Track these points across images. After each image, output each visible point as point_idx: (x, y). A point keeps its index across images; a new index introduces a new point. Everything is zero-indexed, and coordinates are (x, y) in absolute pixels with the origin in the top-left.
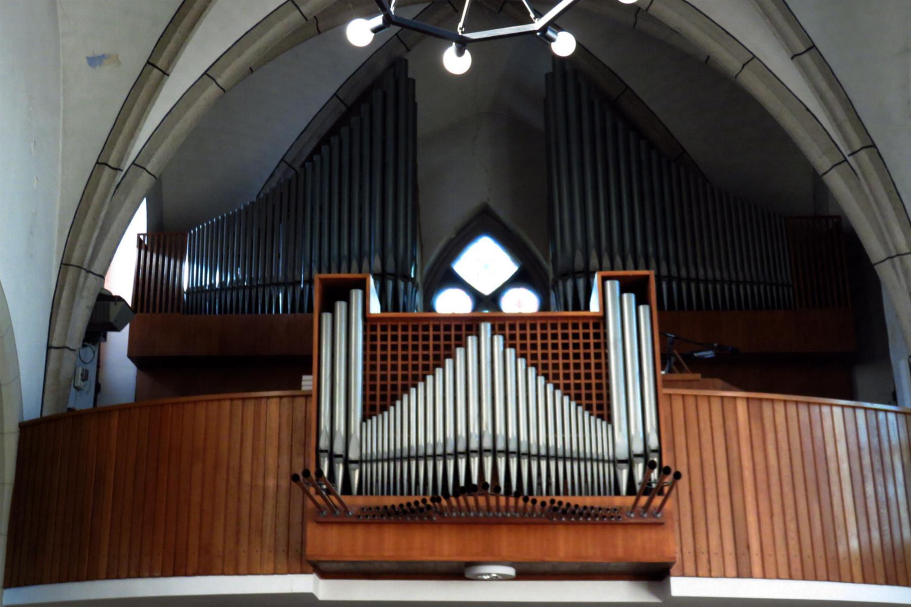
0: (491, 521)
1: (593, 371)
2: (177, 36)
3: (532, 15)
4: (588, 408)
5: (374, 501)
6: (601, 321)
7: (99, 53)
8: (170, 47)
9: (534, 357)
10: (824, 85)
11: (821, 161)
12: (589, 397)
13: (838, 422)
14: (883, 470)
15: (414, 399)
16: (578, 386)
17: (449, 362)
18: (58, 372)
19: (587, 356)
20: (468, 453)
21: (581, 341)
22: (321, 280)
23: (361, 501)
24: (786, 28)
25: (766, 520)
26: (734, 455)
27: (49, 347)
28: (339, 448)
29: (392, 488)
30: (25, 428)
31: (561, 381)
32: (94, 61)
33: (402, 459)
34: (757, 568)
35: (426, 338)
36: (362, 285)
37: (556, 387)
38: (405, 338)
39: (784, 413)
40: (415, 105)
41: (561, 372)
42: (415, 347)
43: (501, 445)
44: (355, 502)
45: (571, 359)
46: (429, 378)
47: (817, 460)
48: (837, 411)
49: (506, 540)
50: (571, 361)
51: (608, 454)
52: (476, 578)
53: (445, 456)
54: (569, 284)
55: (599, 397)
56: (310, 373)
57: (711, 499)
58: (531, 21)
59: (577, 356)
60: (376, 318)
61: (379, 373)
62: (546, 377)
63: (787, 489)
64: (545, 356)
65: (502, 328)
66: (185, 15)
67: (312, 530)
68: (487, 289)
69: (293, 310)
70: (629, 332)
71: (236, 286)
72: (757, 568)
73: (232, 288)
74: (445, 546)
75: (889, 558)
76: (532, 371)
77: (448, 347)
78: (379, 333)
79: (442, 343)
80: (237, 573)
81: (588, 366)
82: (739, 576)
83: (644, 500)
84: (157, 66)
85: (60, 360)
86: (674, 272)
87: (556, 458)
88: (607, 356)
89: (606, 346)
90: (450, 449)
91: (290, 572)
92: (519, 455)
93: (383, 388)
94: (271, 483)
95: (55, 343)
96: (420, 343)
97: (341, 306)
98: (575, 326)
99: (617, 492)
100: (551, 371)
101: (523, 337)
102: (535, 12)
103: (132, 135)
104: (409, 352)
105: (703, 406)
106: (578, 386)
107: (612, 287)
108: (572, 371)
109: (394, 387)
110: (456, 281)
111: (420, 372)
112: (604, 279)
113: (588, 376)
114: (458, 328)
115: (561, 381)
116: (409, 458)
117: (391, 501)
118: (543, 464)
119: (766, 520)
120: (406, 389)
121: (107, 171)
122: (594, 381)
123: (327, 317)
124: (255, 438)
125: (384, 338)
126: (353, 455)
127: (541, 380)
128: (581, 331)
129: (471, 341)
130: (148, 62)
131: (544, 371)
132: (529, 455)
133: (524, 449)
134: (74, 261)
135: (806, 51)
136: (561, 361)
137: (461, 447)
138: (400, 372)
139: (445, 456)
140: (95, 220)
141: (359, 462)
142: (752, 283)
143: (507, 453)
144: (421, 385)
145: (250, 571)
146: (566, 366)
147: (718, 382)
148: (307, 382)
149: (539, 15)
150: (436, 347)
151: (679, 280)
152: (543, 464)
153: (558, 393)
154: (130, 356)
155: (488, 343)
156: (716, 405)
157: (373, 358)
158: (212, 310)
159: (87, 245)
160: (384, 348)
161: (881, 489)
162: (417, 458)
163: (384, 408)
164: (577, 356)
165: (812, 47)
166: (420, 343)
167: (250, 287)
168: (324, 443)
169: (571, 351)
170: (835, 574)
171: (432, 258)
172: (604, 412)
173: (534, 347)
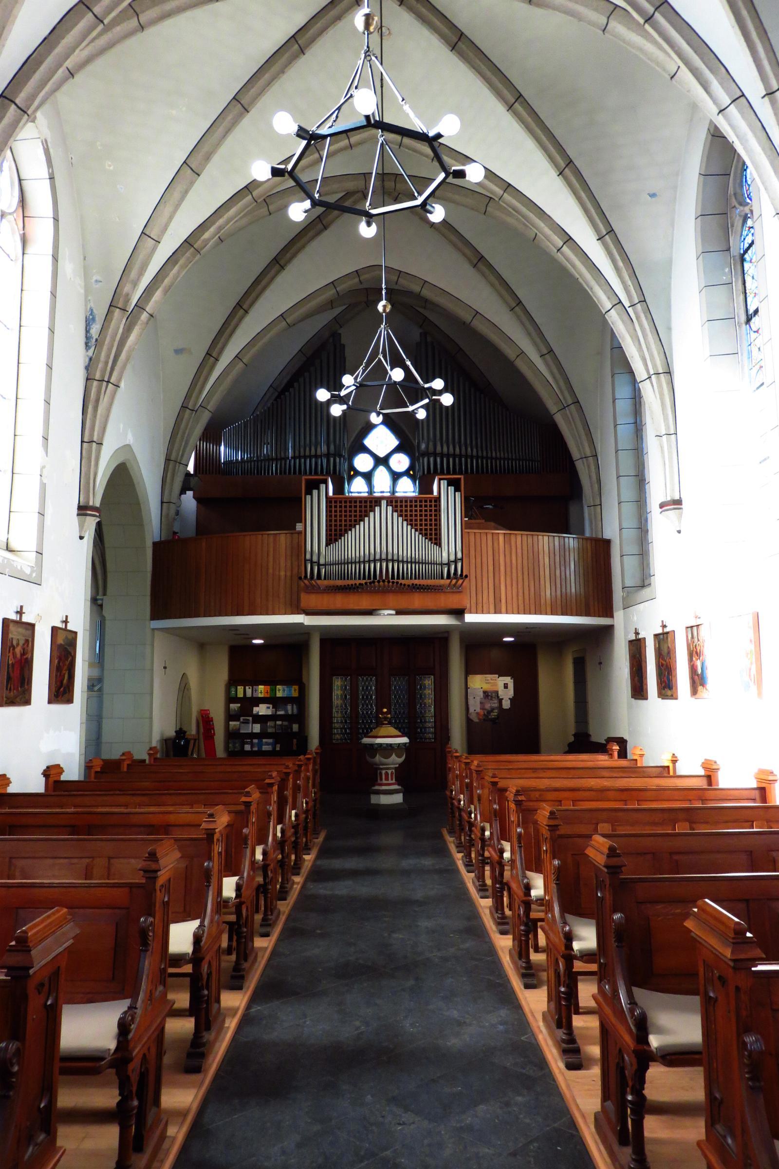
0: (385, 591)
1: (433, 522)
2: (222, 340)
3: (416, 194)
4: (431, 539)
5: (332, 582)
6: (438, 499)
7: (180, 347)
8: (219, 346)
9: (406, 516)
10: (555, 371)
11: (552, 408)
12: (431, 534)
13: (546, 542)
14: (565, 563)
15: (350, 536)
16: (426, 530)
17: (366, 519)
18: (168, 515)
19: (431, 515)
20: (375, 561)
21: (428, 518)
22: (307, 480)
23: (326, 582)
24: (538, 340)
25: (509, 588)
26: (496, 558)
27: (162, 503)
28: (315, 559)
29: (342, 577)
30: (155, 544)
31: (419, 527)
32: (178, 352)
33: (344, 563)
34: (504, 609)
35: (355, 507)
36: (325, 482)
37: (416, 530)
38: (346, 507)
39: (520, 539)
40: (343, 347)
41: (418, 523)
42: (350, 511)
43: (390, 557)
44: (323, 583)
45: (421, 515)
46: (357, 526)
47: (534, 558)
48: (546, 538)
49: (391, 599)
50: (423, 518)
51: (439, 561)
52: (380, 615)
53: (364, 562)
54: (426, 459)
55: (436, 534)
56: (301, 522)
57: (485, 580)
58: (415, 198)
59: (426, 515)
60: (331, 498)
61: (333, 523)
62: (411, 525)
63: (520, 574)
64: (411, 516)
65: (391, 502)
66: (226, 329)
67: (303, 596)
68: (382, 454)
69: (281, 473)
70: (450, 502)
71: (250, 461)
72: (504, 609)
73: (247, 461)
74: (365, 602)
75: (564, 601)
76: (405, 523)
77: (366, 511)
78: (333, 504)
79: (363, 509)
80: (267, 614)
81: (431, 520)
82: (495, 613)
83: (454, 581)
84: (212, 355)
85: (168, 509)
86: (480, 454)
87: (415, 563)
88: (440, 516)
89: (440, 511)
90: (367, 559)
91: (292, 613)
92: (398, 561)
93: (336, 530)
94: (282, 573)
95: (165, 500)
96: (353, 509)
97: (315, 492)
98: (426, 501)
99: (442, 578)
100: (414, 522)
101: (401, 506)
102: (418, 193)
103: (200, 392)
104: (348, 514)
105: (484, 538)
106: (426, 530)
107: (444, 484)
108: (423, 522)
109: (341, 530)
110: (366, 450)
111: (353, 523)
112: (440, 480)
113: (431, 525)
114: (371, 502)
115: (419, 527)
116: (348, 563)
117: (340, 583)
118: (409, 565)
119: (509, 588)
120: (346, 531)
121: (188, 411)
122: (433, 527)
123: (308, 497)
124: (274, 550)
125: (336, 507)
126: (322, 561)
127: (409, 527)
128: (428, 504)
129: (377, 509)
130: (207, 353)
131: (411, 523)
132: (403, 562)
133: (400, 559)
134: (173, 458)
135: (549, 353)
136: (418, 518)
137: (372, 558)
138: (343, 523)
139: (364, 562)
140: (183, 437)
141: (325, 565)
142: (519, 460)
143: (393, 560)
144: (353, 530)
145: (274, 613)
146: (421, 520)
147: (492, 524)
148: (299, 527)
149: (420, 194)
150: (360, 511)
151: (482, 458)
152: (409, 565)
153: (417, 533)
154: (194, 497)
155: (385, 511)
156: (490, 537)
157: (331, 516)
158: (237, 473)
159: (179, 450)
160: (336, 516)
161: (563, 574)
162: (352, 563)
163: (336, 540)
164: (426, 515)
165: (551, 351)
166: (353, 509)
167: (258, 461)
168: (308, 557)
169: (423, 513)
170: (538, 610)
171: (352, 439)
172: (437, 542)
173: (406, 511)
